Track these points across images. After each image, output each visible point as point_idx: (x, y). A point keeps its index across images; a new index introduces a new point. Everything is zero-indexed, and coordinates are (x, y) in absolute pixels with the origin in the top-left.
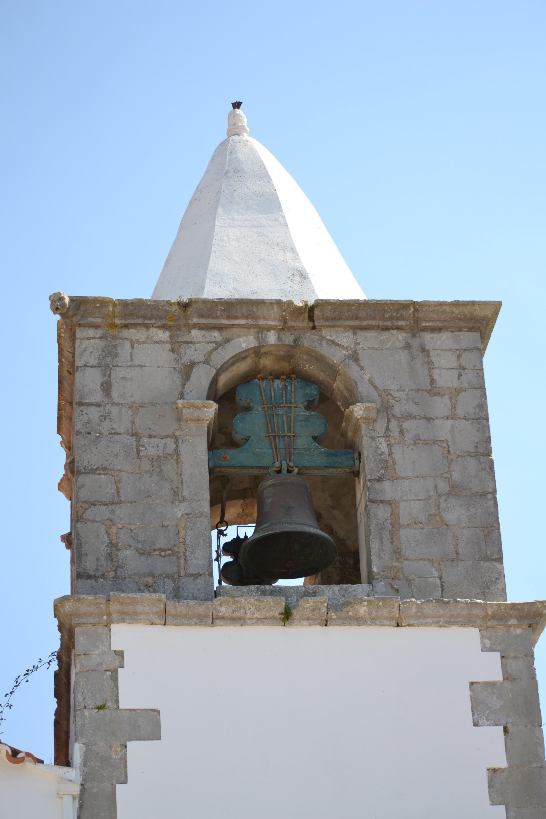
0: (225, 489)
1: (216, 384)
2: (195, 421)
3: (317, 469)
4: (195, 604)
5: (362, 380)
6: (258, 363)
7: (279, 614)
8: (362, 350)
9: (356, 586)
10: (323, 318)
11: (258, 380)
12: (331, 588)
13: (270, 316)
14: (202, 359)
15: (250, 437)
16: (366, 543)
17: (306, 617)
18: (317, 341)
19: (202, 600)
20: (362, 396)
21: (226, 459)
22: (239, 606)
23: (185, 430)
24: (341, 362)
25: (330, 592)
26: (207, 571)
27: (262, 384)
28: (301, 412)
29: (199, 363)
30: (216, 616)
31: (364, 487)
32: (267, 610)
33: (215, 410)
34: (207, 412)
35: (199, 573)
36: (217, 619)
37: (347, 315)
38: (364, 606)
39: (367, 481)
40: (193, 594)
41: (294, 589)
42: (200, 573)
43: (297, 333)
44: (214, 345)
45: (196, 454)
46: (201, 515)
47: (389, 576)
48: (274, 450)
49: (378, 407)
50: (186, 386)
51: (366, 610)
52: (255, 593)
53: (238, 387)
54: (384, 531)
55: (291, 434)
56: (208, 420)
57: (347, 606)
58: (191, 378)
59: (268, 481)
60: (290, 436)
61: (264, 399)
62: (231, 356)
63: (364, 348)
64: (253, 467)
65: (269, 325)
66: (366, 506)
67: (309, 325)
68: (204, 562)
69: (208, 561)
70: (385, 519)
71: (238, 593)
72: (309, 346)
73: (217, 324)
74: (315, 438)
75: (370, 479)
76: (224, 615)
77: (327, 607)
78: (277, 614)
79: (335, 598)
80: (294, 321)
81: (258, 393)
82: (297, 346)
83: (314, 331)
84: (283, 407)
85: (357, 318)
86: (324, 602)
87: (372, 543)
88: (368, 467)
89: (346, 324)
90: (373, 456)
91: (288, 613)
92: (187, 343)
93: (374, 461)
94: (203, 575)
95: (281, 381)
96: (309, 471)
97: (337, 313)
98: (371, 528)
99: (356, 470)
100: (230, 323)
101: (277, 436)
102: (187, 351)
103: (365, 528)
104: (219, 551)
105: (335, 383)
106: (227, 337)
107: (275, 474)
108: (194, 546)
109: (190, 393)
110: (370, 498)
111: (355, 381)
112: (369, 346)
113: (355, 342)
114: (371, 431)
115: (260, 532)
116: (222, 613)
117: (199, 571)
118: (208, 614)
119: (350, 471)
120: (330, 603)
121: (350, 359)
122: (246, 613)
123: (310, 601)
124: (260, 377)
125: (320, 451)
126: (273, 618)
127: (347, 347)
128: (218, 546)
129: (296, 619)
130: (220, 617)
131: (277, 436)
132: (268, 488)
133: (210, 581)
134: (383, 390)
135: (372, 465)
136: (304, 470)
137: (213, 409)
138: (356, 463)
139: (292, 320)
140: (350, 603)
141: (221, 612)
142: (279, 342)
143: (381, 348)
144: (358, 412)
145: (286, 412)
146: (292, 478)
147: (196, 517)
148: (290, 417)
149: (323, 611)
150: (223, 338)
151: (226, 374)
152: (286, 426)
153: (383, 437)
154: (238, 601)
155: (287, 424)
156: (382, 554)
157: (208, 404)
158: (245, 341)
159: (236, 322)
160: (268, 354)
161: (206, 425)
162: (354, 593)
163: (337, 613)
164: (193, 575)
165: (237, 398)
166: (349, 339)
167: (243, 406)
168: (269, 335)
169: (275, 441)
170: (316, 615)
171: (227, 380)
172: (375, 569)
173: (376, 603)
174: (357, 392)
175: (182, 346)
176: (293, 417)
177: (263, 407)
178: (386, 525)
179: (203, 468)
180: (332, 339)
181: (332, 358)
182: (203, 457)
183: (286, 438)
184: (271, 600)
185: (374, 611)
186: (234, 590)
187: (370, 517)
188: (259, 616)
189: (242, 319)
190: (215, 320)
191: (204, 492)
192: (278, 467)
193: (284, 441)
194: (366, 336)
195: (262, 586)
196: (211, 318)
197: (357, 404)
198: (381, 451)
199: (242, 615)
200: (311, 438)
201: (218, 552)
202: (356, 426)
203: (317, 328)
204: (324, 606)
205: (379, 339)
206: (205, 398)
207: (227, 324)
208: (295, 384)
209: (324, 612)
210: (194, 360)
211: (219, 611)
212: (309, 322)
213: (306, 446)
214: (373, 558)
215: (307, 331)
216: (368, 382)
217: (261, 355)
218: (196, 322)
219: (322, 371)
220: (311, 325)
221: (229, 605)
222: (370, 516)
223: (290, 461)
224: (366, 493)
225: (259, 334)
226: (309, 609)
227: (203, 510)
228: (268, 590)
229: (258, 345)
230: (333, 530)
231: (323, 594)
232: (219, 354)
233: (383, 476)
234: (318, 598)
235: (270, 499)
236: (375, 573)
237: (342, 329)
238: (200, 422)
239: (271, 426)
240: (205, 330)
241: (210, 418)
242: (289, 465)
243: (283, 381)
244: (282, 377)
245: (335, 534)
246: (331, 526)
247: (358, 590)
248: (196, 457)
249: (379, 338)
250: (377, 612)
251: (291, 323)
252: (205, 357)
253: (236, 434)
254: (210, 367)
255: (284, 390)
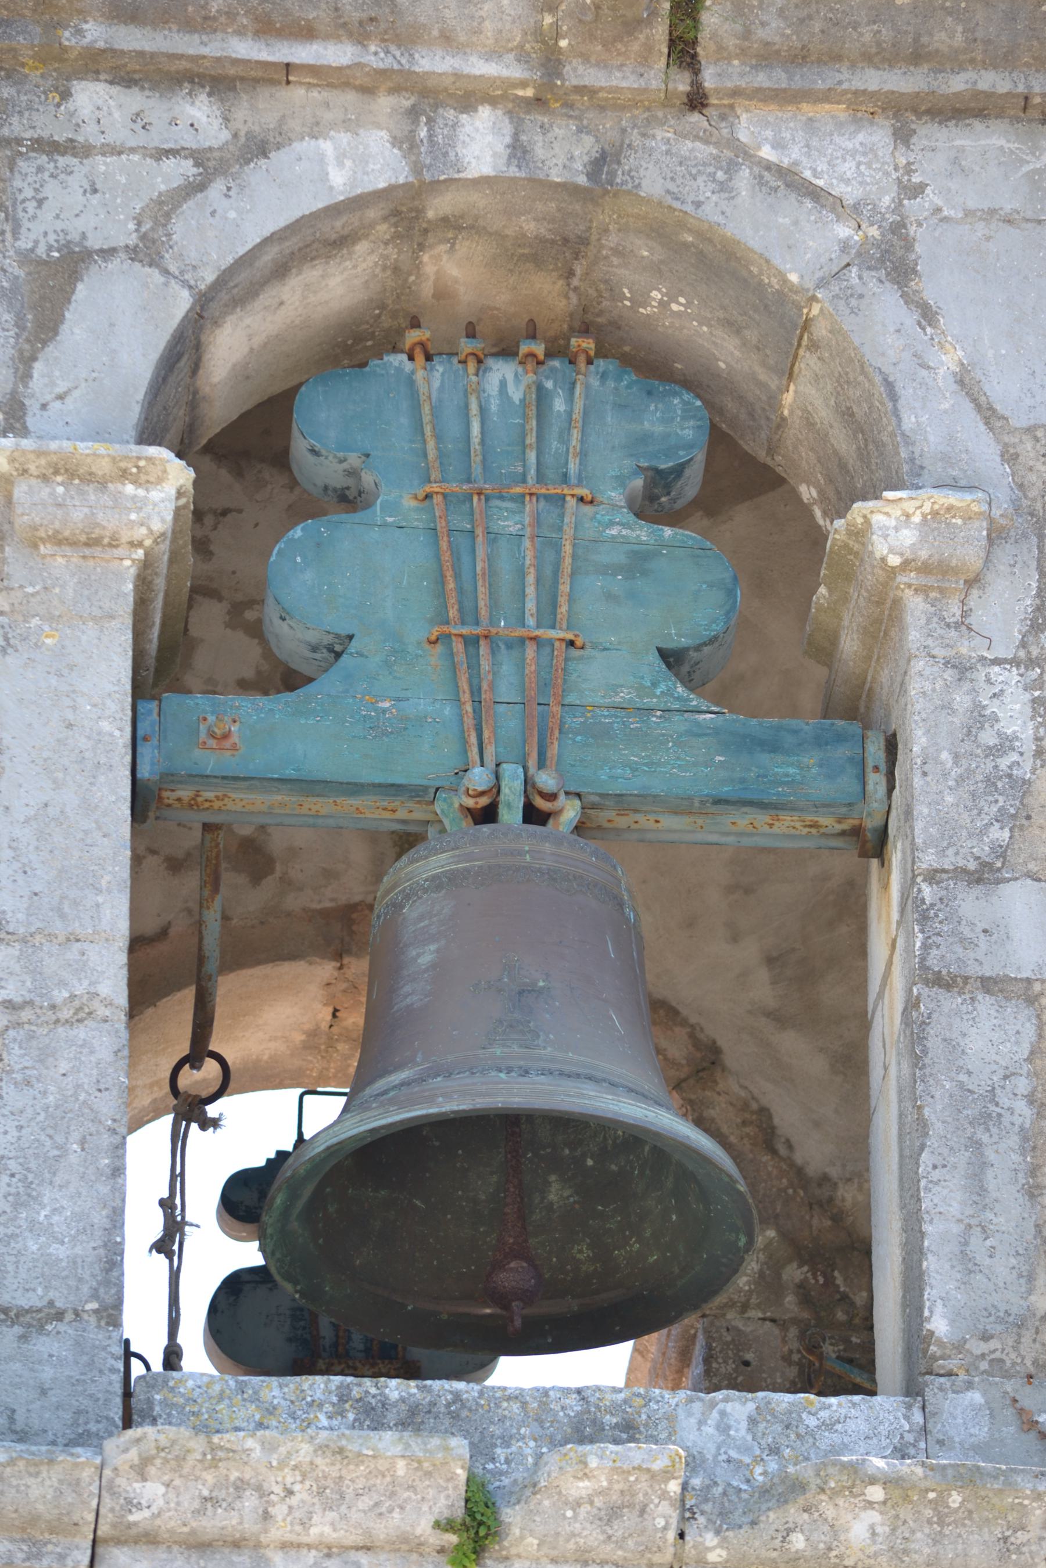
0: (216, 890)
1: (196, 368)
2: (73, 543)
3: (676, 812)
4: (11, 1462)
5: (924, 373)
6: (410, 274)
7: (437, 1525)
8: (934, 220)
9: (840, 1405)
10: (743, 53)
11: (404, 357)
12: (713, 1405)
13: (478, 32)
14: (125, 234)
15: (351, 637)
16: (902, 1188)
17: (571, 1546)
18: (711, 169)
19: (54, 1443)
20: (917, 455)
21: (227, 744)
22: (234, 1475)
23: (21, 587)
24: (822, 283)
25: (709, 1430)
26: (95, 1296)
27: (428, 381)
28: (611, 524)
29: (109, 253)
30: (114, 1526)
31: (902, 911)
32: (377, 1504)
33: (180, 494)
34: (138, 504)
35: (51, 1303)
36: (119, 1542)
37: (868, 37)
38: (870, 1504)
39: (919, 879)
40: (14, 1411)
41: (524, 1405)
42: (58, 1304)
43: (608, 125)
44: (187, 168)
45: (74, 708)
46: (81, 1015)
47: (1008, 1363)
48: (469, 708)
49: (996, 513)
50: (38, 367)
51: (879, 1530)
52: (330, 1418)
53: (303, 389)
54: (994, 1130)
55: (553, 634)
56: (140, 544)
57: (783, 1501)
58: (65, 328)
59: (426, 858)
60: (550, 642)
61: (432, 453)
62: (271, 227)
63: (945, 213)
64: (362, 785)
65: (468, 76)
66: (912, 1004)
67: (671, 86)
68: (78, 1250)
69: (100, 1243)
70: (1001, 1073)
71: (242, 1414)
72: (668, 192)
73: (204, 57)
74: (671, 658)
75: (936, 871)
76: (158, 1522)
77: (683, 1501)
78: (424, 1528)
79: (729, 1461)
80: (597, 65)
81: (404, 420)
82: (606, 192)
83: (695, 117)
84: (523, 496)
85: (917, 56)
86: (668, 1474)
87: (928, 1190)
88: (926, 811)
89: (857, 84)
90: (956, 757)
91: (481, 1524)
92: (51, 148)
93: (960, 780)
94: (69, 1316)
95: (520, 369)
96: (639, 817)
97: (817, 26)
98: (926, 1112)
99: (871, 823)
100: (271, 58)
101: (486, 637)
102: (51, 189)
103: (901, 1115)
104: (178, 1201)
105: (792, 388)
106: (257, 128)
107: (466, 823)
108: (33, 1165)
109: (57, 404)
110: (933, 962)
111: (885, 380)
112: (971, 205)
113: (899, 180)
114: (953, 633)
115: (368, 1109)
116: (146, 1513)
117: (52, 1294)
118: (76, 1518)
119: (839, 827)
120: (696, 1482)
121: (869, 268)
122: (266, 1516)
123: (593, 1462)
124: (415, 344)
125: (697, 723)
126: (404, 1547)
127: (856, 207)
128: (173, 1177)
129: (519, 1556)
130: (134, 1531)
131: (486, 637)
132: (426, 891)
133: (104, 1348)
134: (1030, 430)
135: (949, 799)
136: (611, 814)
137: (169, 489)
138: (870, 787)
139: (586, 58)
140: (798, 1487)
141: (139, 1507)
142: (519, 167)
143: (1029, 214)
144: (892, 532)
145: (537, 521)
146: (548, 847)
147: (57, 1021)
148: (557, 547)
149: (660, 1522)
150: (235, 136)
151: (248, 321)
152: (530, 591)
153: (1015, 662)
154: (229, 1450)
155: (538, 581)
156: (977, 1245)
157: (142, 463)
158: (344, 155)
159: (303, 53)
160: (459, 228)
161: (128, 566)
162: (826, 1440)
163: (730, 1534)
164: (22, 1312)
165: (299, 446)
166: (869, 165)
167: (326, 488)
168: (468, 129)
169: (473, 666)
170: (624, 1539)
171: (252, 350)
172: (939, 1325)
173: (932, 1495)
174: (892, 435)
175: (21, 164)
176: (568, 549)
177: (421, 494)
178: (1004, 1101)
179: (102, 779)
180: (786, 162)
181: (777, 261)
182: (105, 726)
183: (530, 651)
184: (398, 1449)
185: (919, 1535)
186: (221, 1397)
187: (927, 1061)
188: (335, 1535)
189: (338, 38)
190: (196, 36)
191: (100, 899)
192: (482, 793)
193: (521, 665)
194: (961, 150)
195: (367, 1382)
196: (174, 27)
197: (889, 495)
198: (999, 734)
199: (250, 1526)
200: (654, 658)
201: (173, 1207)
202: (879, 603)
203: (713, 101)
204: (664, 1495)
205: (1025, 169)
206: (132, 433)
207: (258, 62)
208: (587, 387)
209: (665, 1528)
210: (84, 236)
211: (129, 1501)
212: (674, 69)
213: (624, 695)
214: (930, 1264)
215: (660, 114)
216: (955, 387)
217: (426, 231)
218: (101, 44)
219: (729, 324)
220: (682, 84)
221: (185, 1471)
222: (925, 1052)
223: (541, 765)
224: (910, 936)
225: (416, 122)
226: (588, 1507)
227: (92, 990)
228: (395, 1404)
229: (411, 179)
230: (773, 1128)
231: (670, 1434)
232: (213, 213)
233: (1003, 856)
234: (635, 1453)
235: (433, 947)
236: (940, 1343)
237: (840, 110)
238: (97, 551)
239: (460, 591)
240: (142, 88)
241: (151, 531)
242: (534, 786)
243: (529, 367)
244: (524, 348)
245: (783, 1151)
246: (764, 1112)
247: (851, 1425)
248: (70, 726)
249: (1028, 162)
250: (935, 1542)
251: (581, 69)
252: (139, 224)
253: (284, 619)
254: (162, 279)
255: (533, 412)
